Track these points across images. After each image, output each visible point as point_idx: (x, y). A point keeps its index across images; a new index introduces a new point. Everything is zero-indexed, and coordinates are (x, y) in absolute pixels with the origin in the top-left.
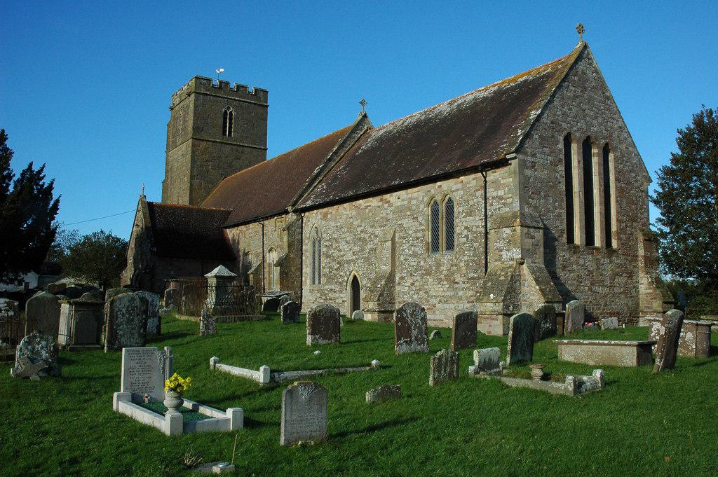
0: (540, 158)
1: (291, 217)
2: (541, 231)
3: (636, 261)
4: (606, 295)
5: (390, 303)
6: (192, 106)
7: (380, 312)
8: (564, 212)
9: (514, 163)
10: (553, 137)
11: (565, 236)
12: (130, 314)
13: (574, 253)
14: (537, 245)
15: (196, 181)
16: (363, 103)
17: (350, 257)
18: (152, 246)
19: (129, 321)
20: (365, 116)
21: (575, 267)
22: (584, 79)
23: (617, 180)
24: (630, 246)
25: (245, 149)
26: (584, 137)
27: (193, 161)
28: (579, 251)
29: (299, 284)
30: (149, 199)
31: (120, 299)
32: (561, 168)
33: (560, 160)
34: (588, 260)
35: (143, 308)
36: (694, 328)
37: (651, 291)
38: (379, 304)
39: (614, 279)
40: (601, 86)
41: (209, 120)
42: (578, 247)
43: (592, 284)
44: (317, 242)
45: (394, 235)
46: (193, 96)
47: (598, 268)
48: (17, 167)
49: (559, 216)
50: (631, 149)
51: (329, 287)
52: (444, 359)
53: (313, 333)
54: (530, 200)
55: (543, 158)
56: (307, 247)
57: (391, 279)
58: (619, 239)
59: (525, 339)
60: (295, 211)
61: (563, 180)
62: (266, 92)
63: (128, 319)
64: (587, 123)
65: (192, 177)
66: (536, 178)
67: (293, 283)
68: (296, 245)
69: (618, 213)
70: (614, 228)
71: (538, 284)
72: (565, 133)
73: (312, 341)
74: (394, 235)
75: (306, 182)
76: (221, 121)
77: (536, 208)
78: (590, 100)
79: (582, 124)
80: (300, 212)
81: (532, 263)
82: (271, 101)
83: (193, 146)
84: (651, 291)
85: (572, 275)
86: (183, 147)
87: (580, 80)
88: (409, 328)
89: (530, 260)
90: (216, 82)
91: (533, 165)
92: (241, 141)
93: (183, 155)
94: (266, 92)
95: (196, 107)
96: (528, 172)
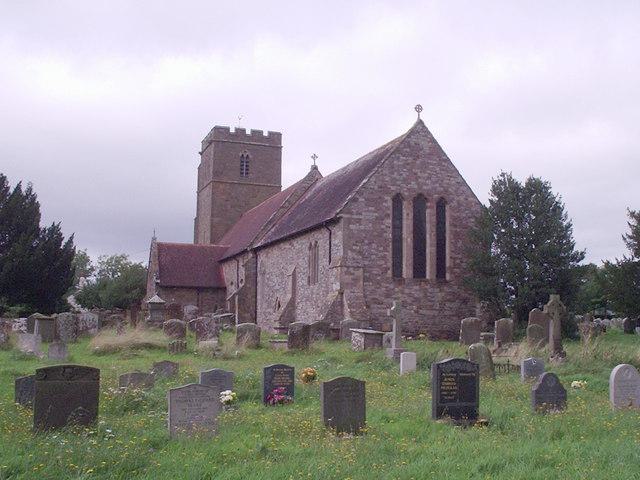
8: (389, 255)
9: (342, 221)
11: (390, 272)
17: (277, 287)
19: (66, 329)
20: (315, 168)
26: (414, 194)
30: (158, 241)
33: (389, 215)
34: (415, 290)
42: (404, 280)
46: (213, 145)
47: (426, 296)
49: (384, 257)
54: (354, 247)
57: (292, 304)
62: (279, 135)
64: (418, 184)
67: (249, 308)
68: (252, 278)
70: (448, 263)
72: (394, 194)
80: (256, 251)
90: (232, 130)
94: (279, 135)
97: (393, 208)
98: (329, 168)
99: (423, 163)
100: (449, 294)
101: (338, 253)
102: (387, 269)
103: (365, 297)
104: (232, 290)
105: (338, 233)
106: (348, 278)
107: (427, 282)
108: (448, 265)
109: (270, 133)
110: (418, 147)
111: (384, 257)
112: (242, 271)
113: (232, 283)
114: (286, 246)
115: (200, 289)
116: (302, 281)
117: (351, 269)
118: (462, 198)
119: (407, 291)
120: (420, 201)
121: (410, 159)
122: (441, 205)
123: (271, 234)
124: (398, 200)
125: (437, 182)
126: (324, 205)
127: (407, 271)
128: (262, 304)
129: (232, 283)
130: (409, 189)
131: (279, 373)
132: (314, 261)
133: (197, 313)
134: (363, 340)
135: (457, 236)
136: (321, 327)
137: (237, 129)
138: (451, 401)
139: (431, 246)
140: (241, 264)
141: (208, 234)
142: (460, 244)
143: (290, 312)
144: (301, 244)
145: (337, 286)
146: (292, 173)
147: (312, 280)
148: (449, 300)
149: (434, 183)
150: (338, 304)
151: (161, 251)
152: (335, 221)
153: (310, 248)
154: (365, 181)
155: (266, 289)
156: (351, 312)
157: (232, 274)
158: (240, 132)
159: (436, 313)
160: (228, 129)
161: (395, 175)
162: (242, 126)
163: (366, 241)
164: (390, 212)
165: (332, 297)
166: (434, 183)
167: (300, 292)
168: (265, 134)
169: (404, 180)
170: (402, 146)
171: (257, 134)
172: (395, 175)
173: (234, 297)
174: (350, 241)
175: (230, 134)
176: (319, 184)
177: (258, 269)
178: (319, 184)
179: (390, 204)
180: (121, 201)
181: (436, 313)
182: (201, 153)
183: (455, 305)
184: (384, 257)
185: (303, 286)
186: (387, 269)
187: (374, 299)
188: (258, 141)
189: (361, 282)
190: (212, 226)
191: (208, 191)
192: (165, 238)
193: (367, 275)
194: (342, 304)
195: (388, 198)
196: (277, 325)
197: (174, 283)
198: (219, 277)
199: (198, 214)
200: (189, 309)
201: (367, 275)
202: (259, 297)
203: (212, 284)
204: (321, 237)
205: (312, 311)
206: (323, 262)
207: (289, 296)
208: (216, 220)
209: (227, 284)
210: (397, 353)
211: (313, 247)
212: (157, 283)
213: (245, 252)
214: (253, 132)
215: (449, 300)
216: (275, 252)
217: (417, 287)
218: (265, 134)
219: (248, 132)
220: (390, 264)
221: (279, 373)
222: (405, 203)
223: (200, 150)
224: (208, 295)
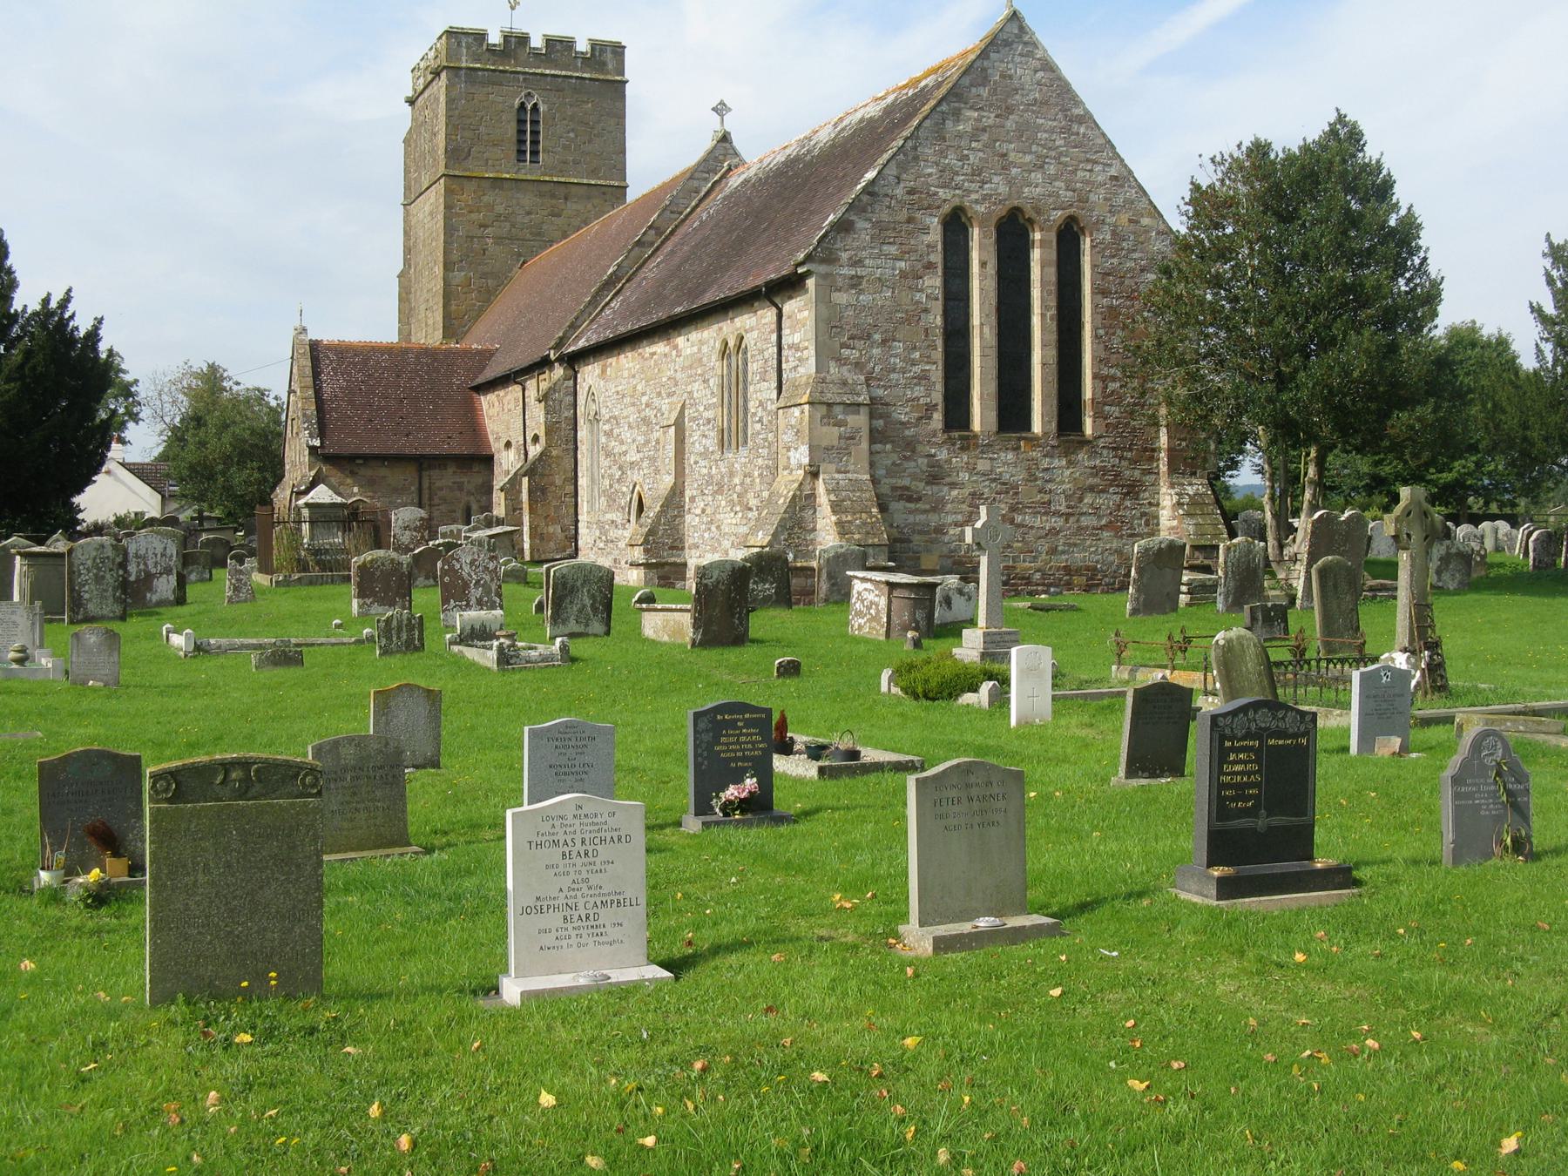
0: (873, 267)
1: (559, 371)
2: (864, 411)
3: (1152, 459)
4: (1054, 532)
5: (672, 548)
6: (442, 98)
7: (647, 566)
8: (937, 373)
9: (811, 283)
10: (910, 220)
11: (938, 417)
12: (99, 569)
13: (962, 449)
14: (852, 438)
15: (458, 276)
16: (721, 109)
17: (633, 456)
18: (311, 436)
19: (99, 579)
20: (725, 138)
21: (964, 476)
22: (1008, 86)
23: (1099, 291)
24: (1134, 429)
25: (574, 189)
26: (1001, 210)
27: (449, 229)
28: (977, 446)
29: (572, 510)
30: (313, 335)
31: (82, 546)
32: (934, 282)
33: (930, 266)
34: (1007, 463)
35: (118, 560)
36: (886, 589)
37: (1175, 523)
38: (646, 551)
39: (1081, 499)
40: (1060, 94)
41: (482, 129)
42: (976, 436)
43: (1013, 509)
45: (682, 412)
46: (443, 75)
47: (1032, 478)
48: (26, 299)
49: (923, 377)
50: (1145, 221)
51: (609, 516)
52: (395, 623)
53: (361, 595)
55: (883, 264)
57: (674, 501)
58: (1098, 415)
59: (588, 602)
60: (560, 359)
61: (937, 308)
62: (618, 50)
63: (96, 575)
64: (1010, 182)
65: (448, 266)
66: (859, 309)
68: (563, 430)
69: (1098, 361)
71: (834, 512)
72: (947, 208)
73: (360, 607)
74: (682, 412)
75: (585, 295)
76: (512, 128)
77: (858, 365)
78: (1025, 133)
79: (998, 185)
80: (574, 361)
81: (839, 472)
82: (634, 69)
83: (449, 192)
84: (1175, 523)
85: (955, 493)
86: (432, 193)
87: (994, 92)
88: (466, 585)
89: (833, 467)
90: (495, 38)
91: (855, 283)
92: (561, 173)
93: (431, 213)
94: (618, 50)
95: (450, 101)
96: (841, 298)
97: (945, 244)
98: (762, 144)
99: (1021, 130)
100: (1095, 472)
101: (803, 367)
102: (931, 408)
103: (875, 481)
104: (508, 462)
105: (800, 310)
106: (831, 434)
107: (1034, 441)
108: (1088, 394)
109: (595, 45)
110: (1001, 79)
111: (923, 377)
112: (537, 414)
113: (508, 445)
114: (660, 348)
115: (423, 462)
116: (701, 440)
117: (838, 409)
118: (1124, 218)
119: (982, 465)
120: (1012, 235)
121: (990, 119)
122: (1068, 239)
123: (613, 318)
124: (956, 225)
125: (1056, 178)
126: (743, 244)
127: (981, 414)
128: (591, 502)
129: (508, 445)
130: (984, 203)
131: (732, 724)
132: (735, 388)
133: (428, 528)
134: (883, 602)
135: (1109, 317)
136: (768, 565)
137: (507, 38)
138: (1245, 812)
139: (1044, 345)
140: (532, 393)
141: (438, 316)
142: (1116, 343)
143: (669, 523)
144: (700, 343)
145: (801, 456)
146: (657, 150)
147: (733, 435)
148: (1091, 489)
149: (1052, 179)
150: (802, 503)
151: (318, 358)
152: (791, 284)
153: (724, 352)
154: (870, 175)
155: (605, 463)
156: (839, 523)
157: (509, 422)
158: (516, 42)
159: (1057, 522)
160: (481, 36)
161: (951, 159)
162: (520, 27)
163: (877, 337)
164: (937, 258)
165: (787, 484)
166: (1052, 179)
167: (698, 468)
168: (582, 46)
169: (976, 172)
170: (966, 81)
171: (559, 47)
172: (951, 159)
173: (514, 483)
174: (830, 330)
175: (491, 50)
176: (735, 181)
177: (580, 409)
178: (735, 181)
179: (935, 235)
180: (231, 242)
181: (1057, 522)
182: (411, 102)
183: (1109, 500)
184: (917, 386)
185: (705, 454)
186: (931, 408)
187: (894, 489)
188: (910, 116)
189: (865, 445)
190: (448, 296)
191: (434, 199)
192: (328, 332)
193: (880, 423)
194: (812, 496)
195: (935, 222)
196: (638, 554)
197: (350, 445)
198: (474, 428)
199: (407, 262)
200: (404, 517)
201: (880, 423)
202: (583, 482)
203: (458, 447)
204: (754, 324)
205: (730, 521)
206: (762, 392)
207: (668, 480)
208: (458, 276)
209: (496, 446)
210: (996, 650)
211: (734, 352)
212: (312, 449)
213: (544, 364)
214: (550, 42)
215: (1091, 489)
216: (626, 362)
217: (1010, 456)
218: (582, 46)
219: (537, 42)
220: (937, 396)
221: (732, 724)
222: (975, 233)
223: (410, 94)
224: (445, 479)
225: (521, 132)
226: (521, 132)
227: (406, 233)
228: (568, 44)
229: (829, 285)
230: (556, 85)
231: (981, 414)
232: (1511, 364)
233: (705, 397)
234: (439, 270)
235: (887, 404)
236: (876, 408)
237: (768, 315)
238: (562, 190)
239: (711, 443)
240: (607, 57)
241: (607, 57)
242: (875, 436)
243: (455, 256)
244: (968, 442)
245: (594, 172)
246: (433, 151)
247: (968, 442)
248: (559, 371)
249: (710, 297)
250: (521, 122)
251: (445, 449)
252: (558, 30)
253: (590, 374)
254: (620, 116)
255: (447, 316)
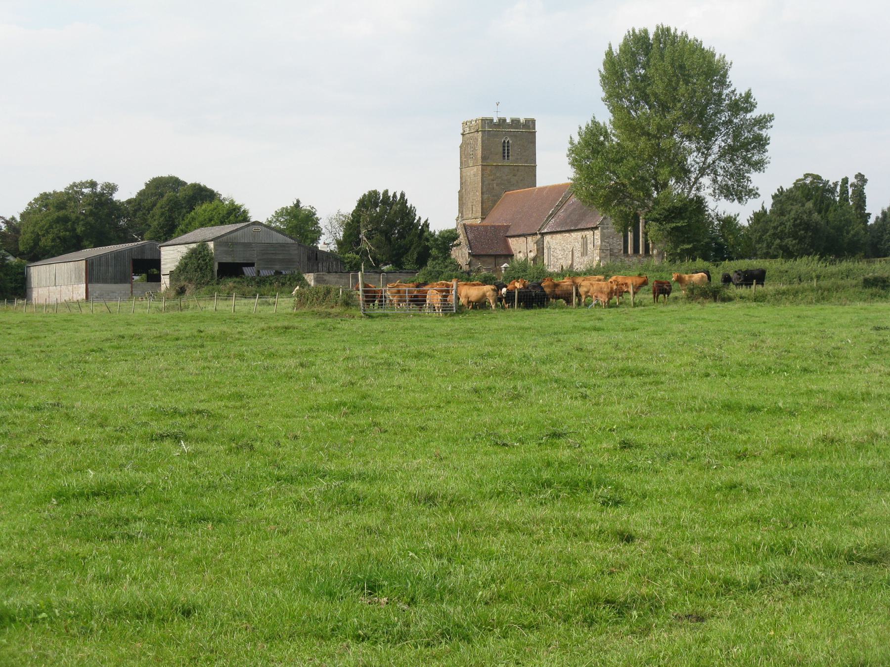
1: (539, 236)
8: (622, 243)
34: (635, 259)
44: (549, 248)
56: (545, 251)
62: (533, 122)
76: (501, 149)
101: (598, 242)
105: (598, 233)
114: (567, 235)
116: (577, 254)
127: (630, 250)
144: (578, 235)
145: (598, 258)
152: (596, 228)
158: (502, 121)
190: (482, 203)
197: (478, 252)
198: (508, 247)
203: (504, 252)
204: (589, 234)
206: (590, 246)
208: (486, 196)
213: (536, 234)
219: (508, 121)
225: (504, 150)
226: (504, 150)
227: (461, 178)
228: (518, 121)
229: (603, 229)
230: (514, 136)
231: (630, 250)
232: (316, 240)
233: (578, 246)
234: (479, 194)
235: (682, 256)
236: (611, 250)
237: (592, 232)
238: (516, 168)
239: (580, 255)
240: (530, 125)
241: (530, 125)
242: (611, 255)
243: (485, 190)
244: (628, 256)
245: (526, 162)
246: (475, 155)
247: (628, 256)
248: (539, 236)
249: (579, 227)
250: (504, 147)
251: (502, 253)
252: (515, 116)
253: (547, 238)
254: (534, 143)
255: (482, 209)
